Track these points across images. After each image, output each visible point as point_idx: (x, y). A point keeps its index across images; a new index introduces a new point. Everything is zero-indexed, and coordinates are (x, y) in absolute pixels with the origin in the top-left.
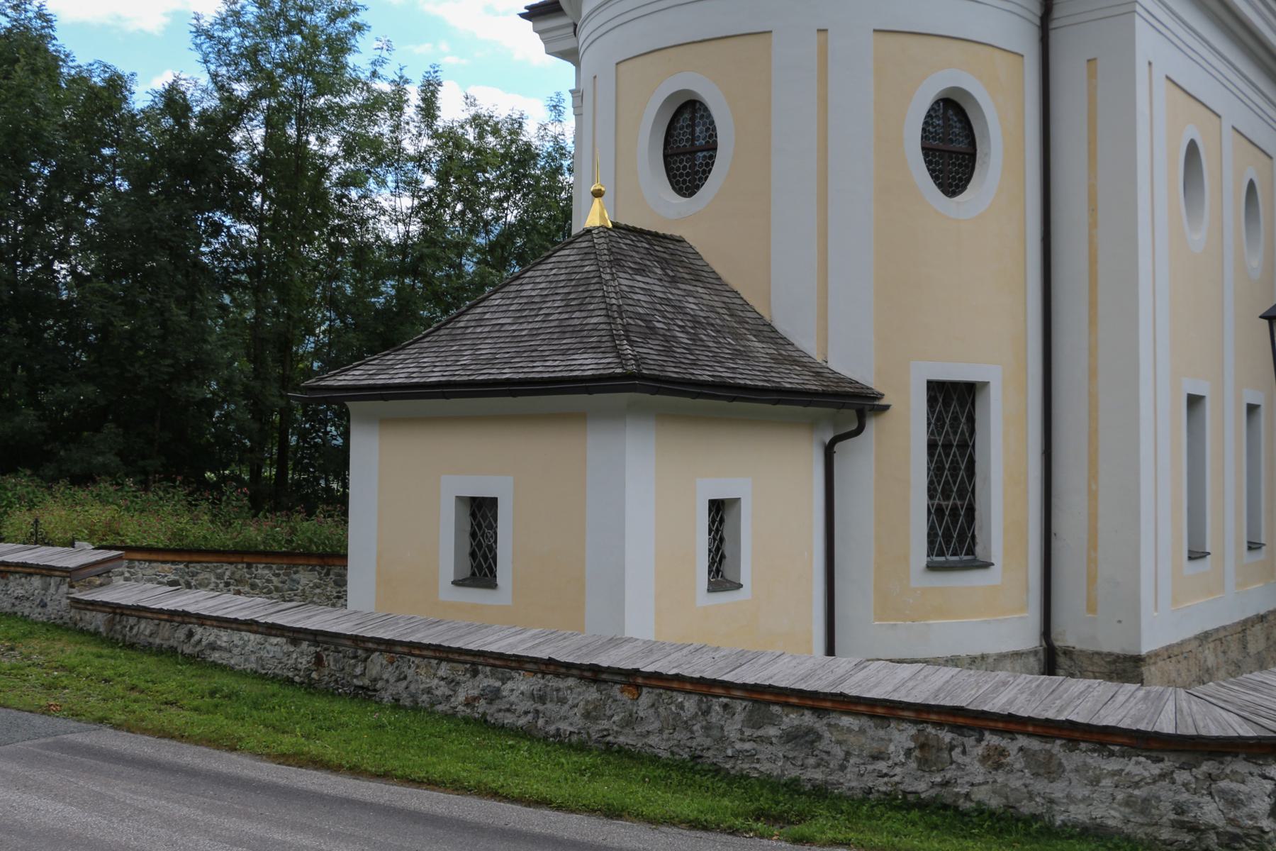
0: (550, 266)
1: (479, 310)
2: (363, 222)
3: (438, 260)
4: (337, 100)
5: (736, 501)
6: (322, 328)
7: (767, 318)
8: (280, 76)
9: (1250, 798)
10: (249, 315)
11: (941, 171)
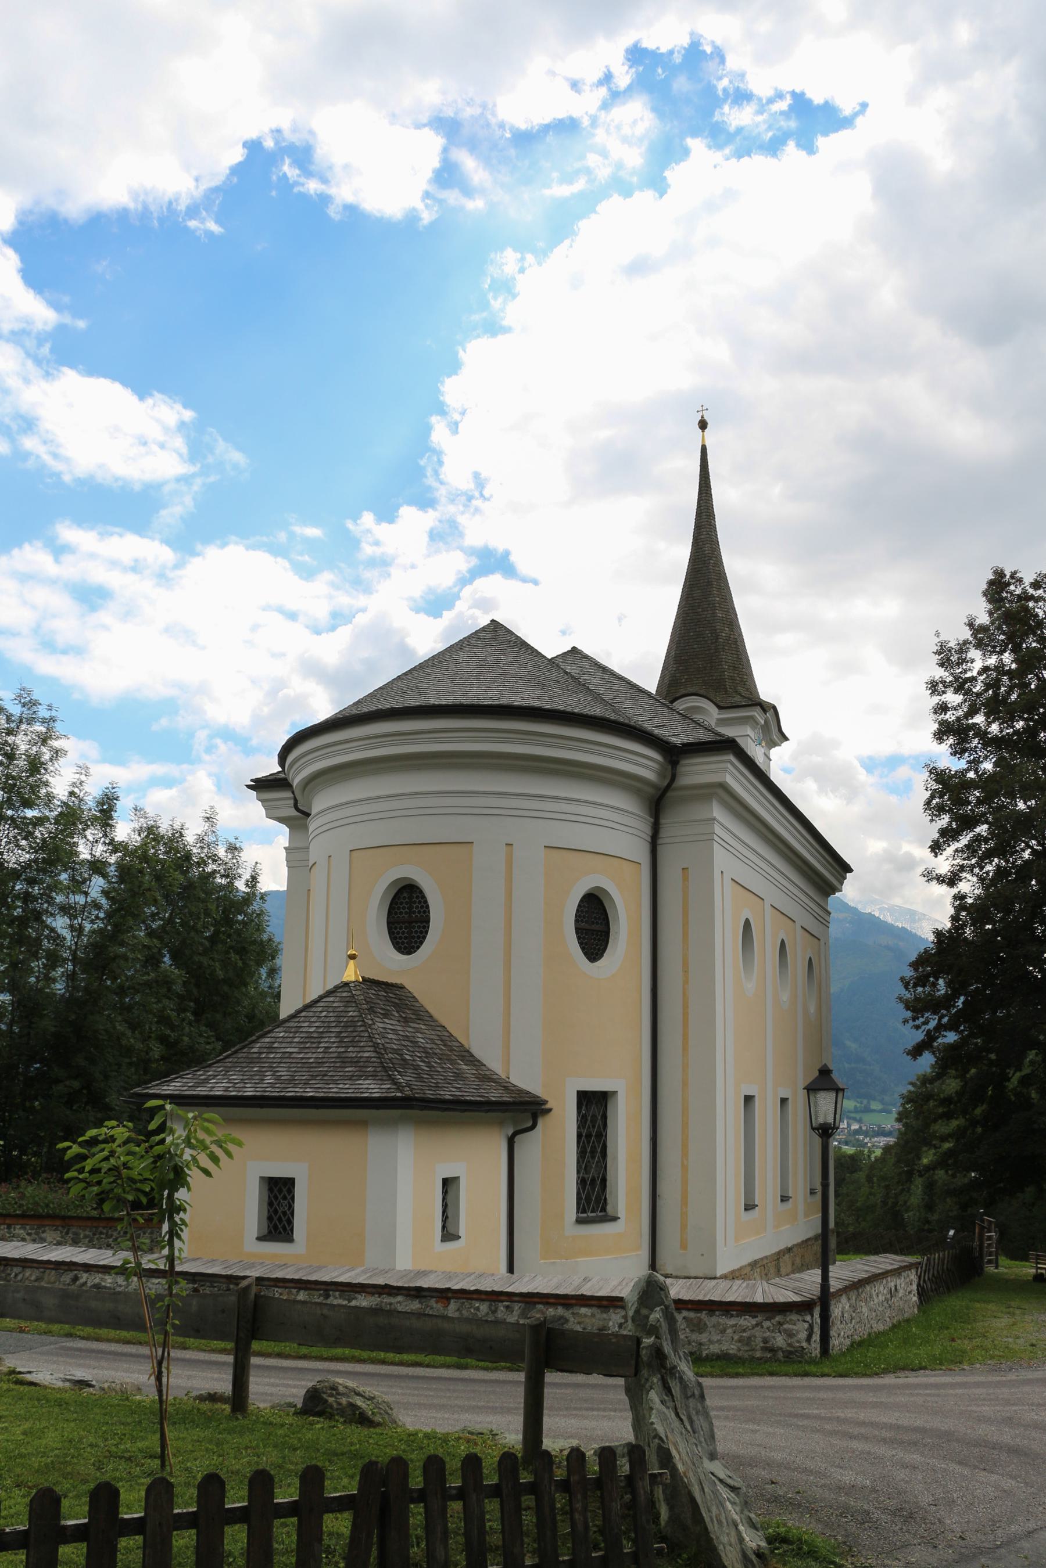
0: (320, 1009)
7: (466, 1046)
9: (798, 1332)
11: (586, 944)
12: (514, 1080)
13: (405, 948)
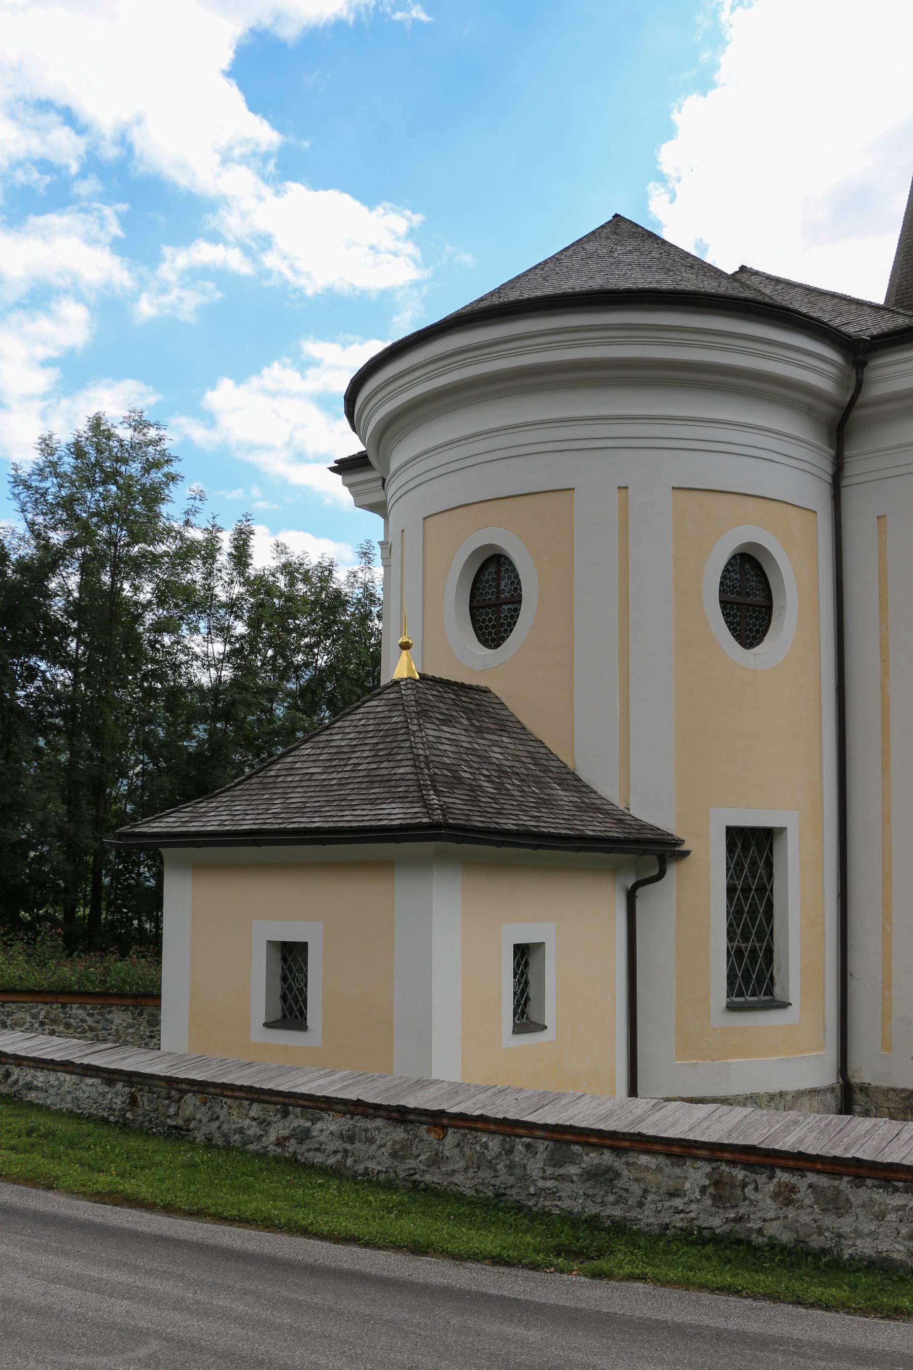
0: (359, 717)
1: (290, 759)
2: (176, 667)
3: (249, 705)
4: (151, 548)
5: (540, 945)
6: (136, 771)
7: (571, 766)
8: (96, 525)
10: (63, 758)
11: (738, 624)
12: (636, 812)
13: (493, 640)
